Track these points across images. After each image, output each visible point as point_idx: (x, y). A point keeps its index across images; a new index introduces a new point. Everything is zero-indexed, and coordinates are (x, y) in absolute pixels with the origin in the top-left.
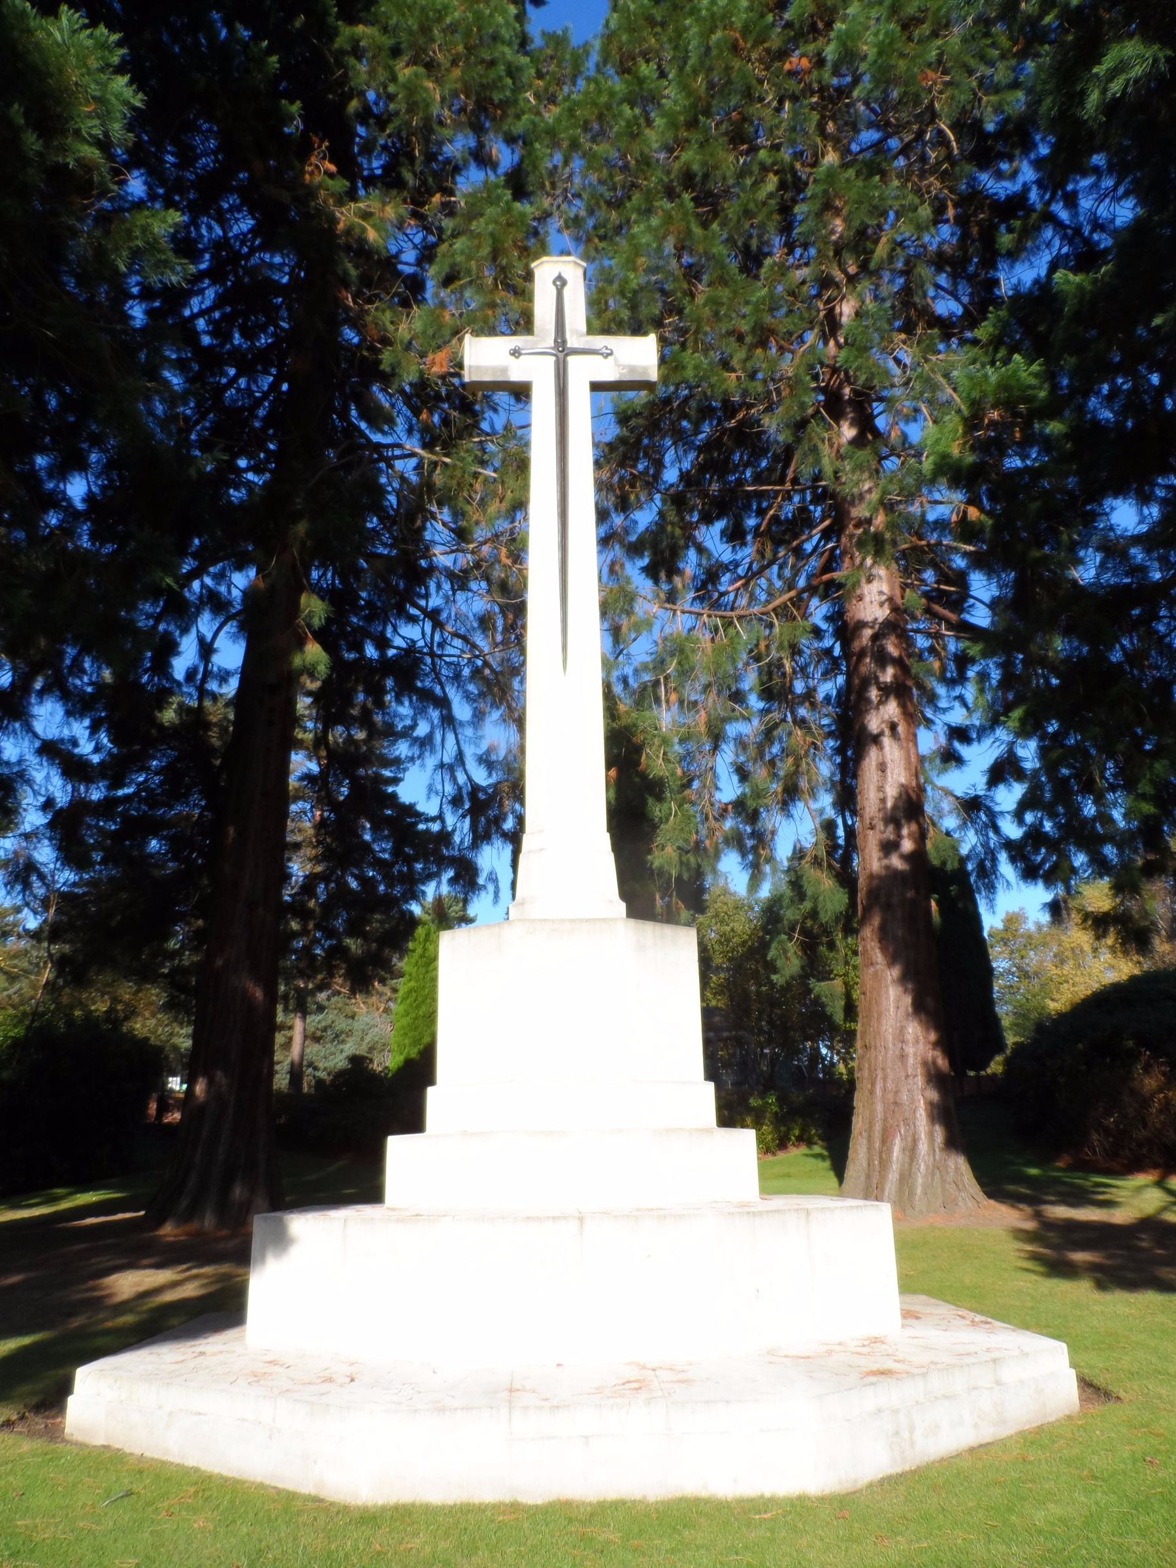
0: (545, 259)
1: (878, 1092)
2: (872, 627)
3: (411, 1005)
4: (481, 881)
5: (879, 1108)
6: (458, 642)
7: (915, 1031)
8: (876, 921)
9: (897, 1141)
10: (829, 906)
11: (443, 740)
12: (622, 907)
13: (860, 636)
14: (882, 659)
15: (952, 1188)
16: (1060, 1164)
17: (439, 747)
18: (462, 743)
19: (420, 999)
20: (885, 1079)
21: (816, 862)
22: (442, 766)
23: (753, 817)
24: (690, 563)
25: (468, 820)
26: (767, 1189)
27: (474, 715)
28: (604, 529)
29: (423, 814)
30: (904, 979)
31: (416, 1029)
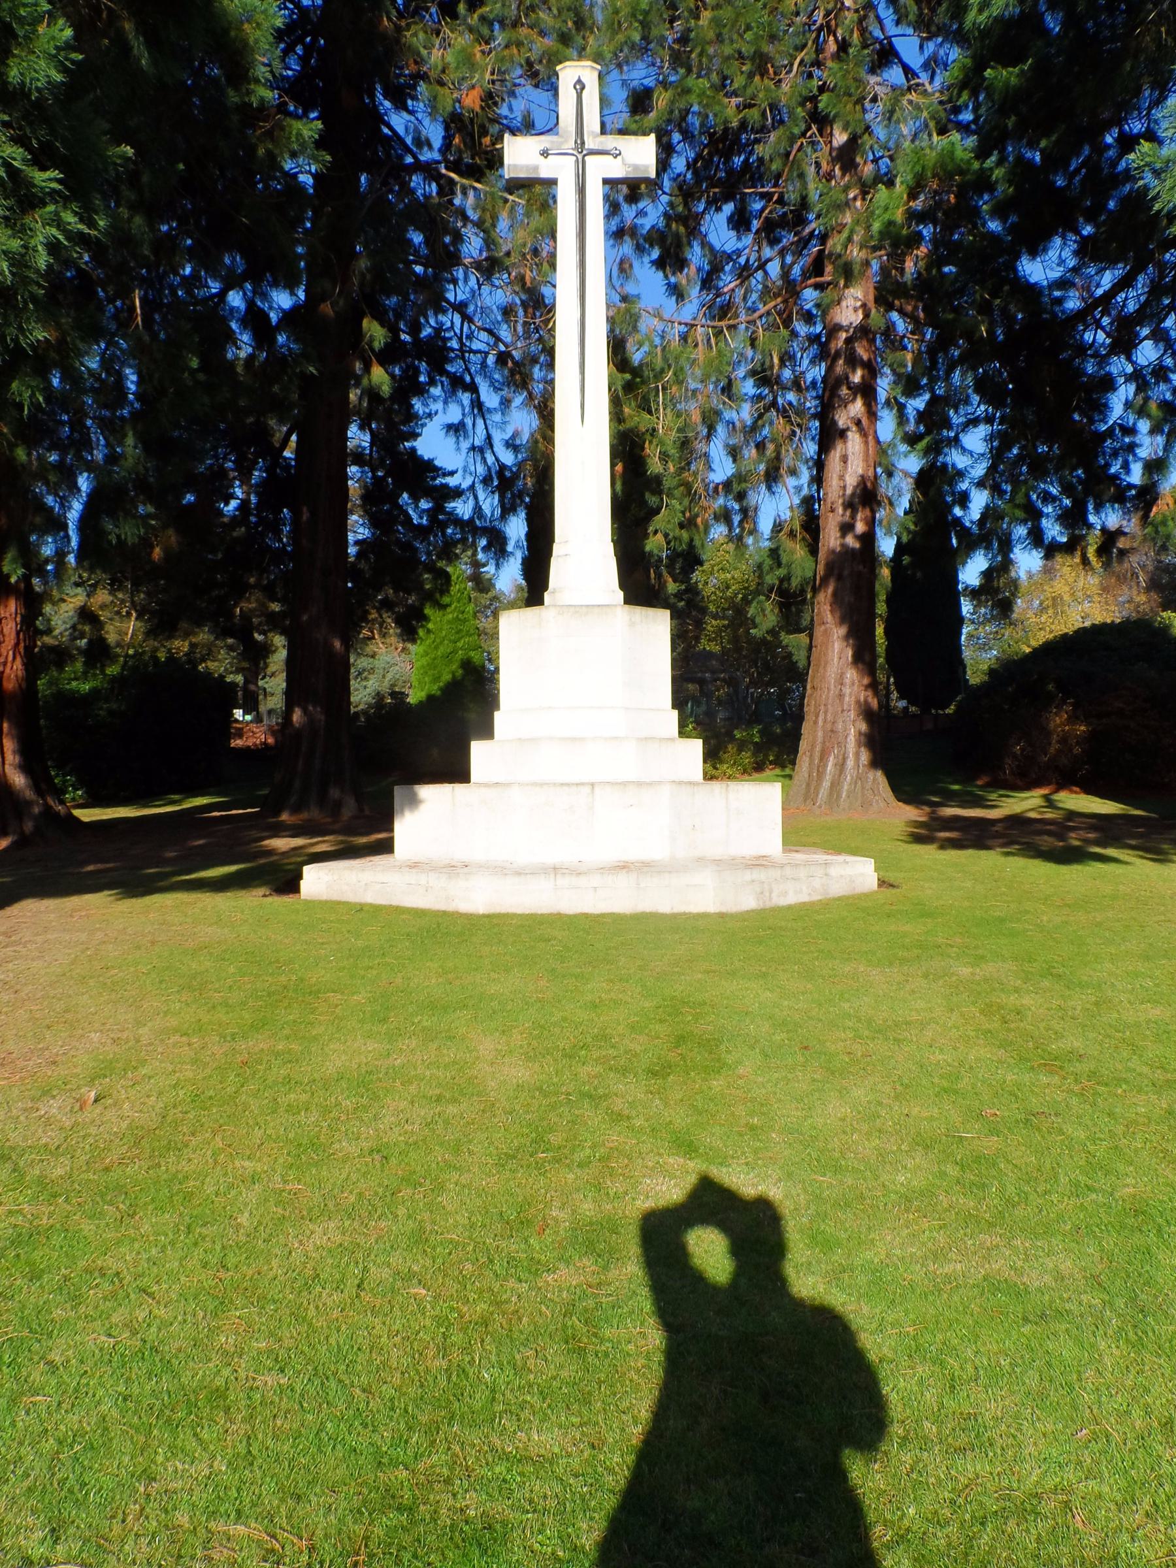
0: (567, 63)
1: (820, 723)
2: (847, 331)
3: (430, 646)
4: (510, 548)
5: (820, 734)
6: (484, 336)
7: (851, 674)
8: (830, 590)
9: (831, 758)
10: (799, 573)
11: (474, 425)
12: (621, 594)
13: (837, 339)
14: (853, 361)
15: (869, 793)
16: (979, 783)
17: (471, 433)
18: (490, 427)
19: (438, 640)
20: (826, 712)
21: (792, 534)
22: (473, 448)
23: (741, 496)
24: (696, 255)
25: (497, 496)
26: (708, 777)
27: (501, 403)
28: (614, 224)
29: (441, 468)
30: (847, 637)
31: (435, 668)
